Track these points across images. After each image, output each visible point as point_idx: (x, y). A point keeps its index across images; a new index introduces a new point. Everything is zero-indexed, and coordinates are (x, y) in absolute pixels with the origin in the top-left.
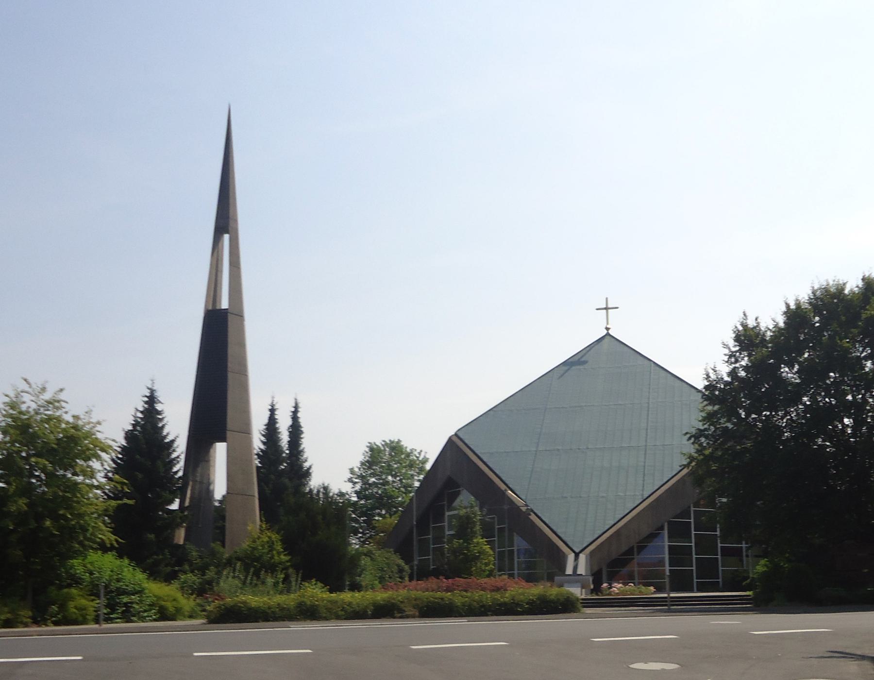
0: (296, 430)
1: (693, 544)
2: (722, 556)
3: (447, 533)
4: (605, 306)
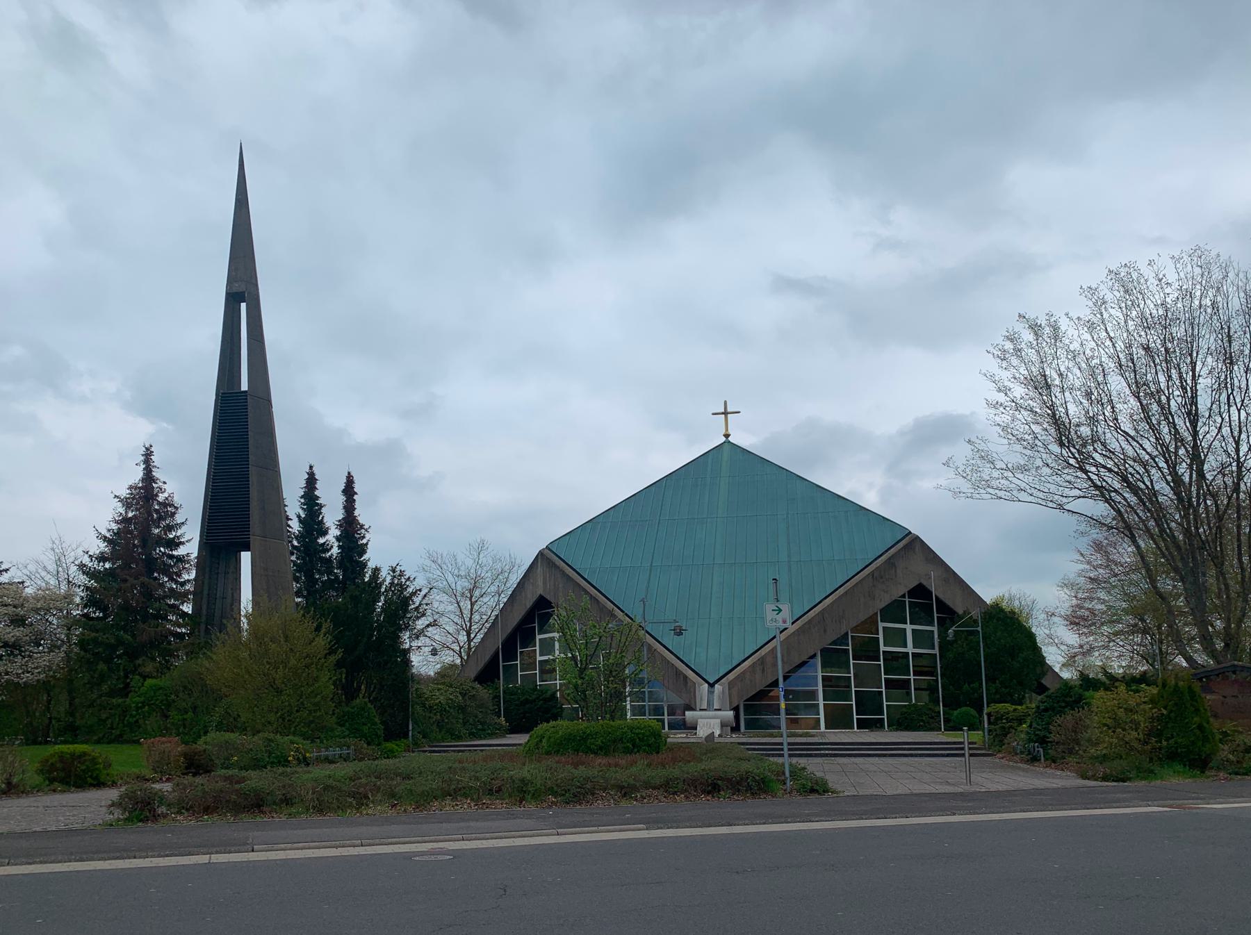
0: (350, 526)
1: (852, 675)
2: (886, 688)
3: (539, 658)
4: (723, 411)
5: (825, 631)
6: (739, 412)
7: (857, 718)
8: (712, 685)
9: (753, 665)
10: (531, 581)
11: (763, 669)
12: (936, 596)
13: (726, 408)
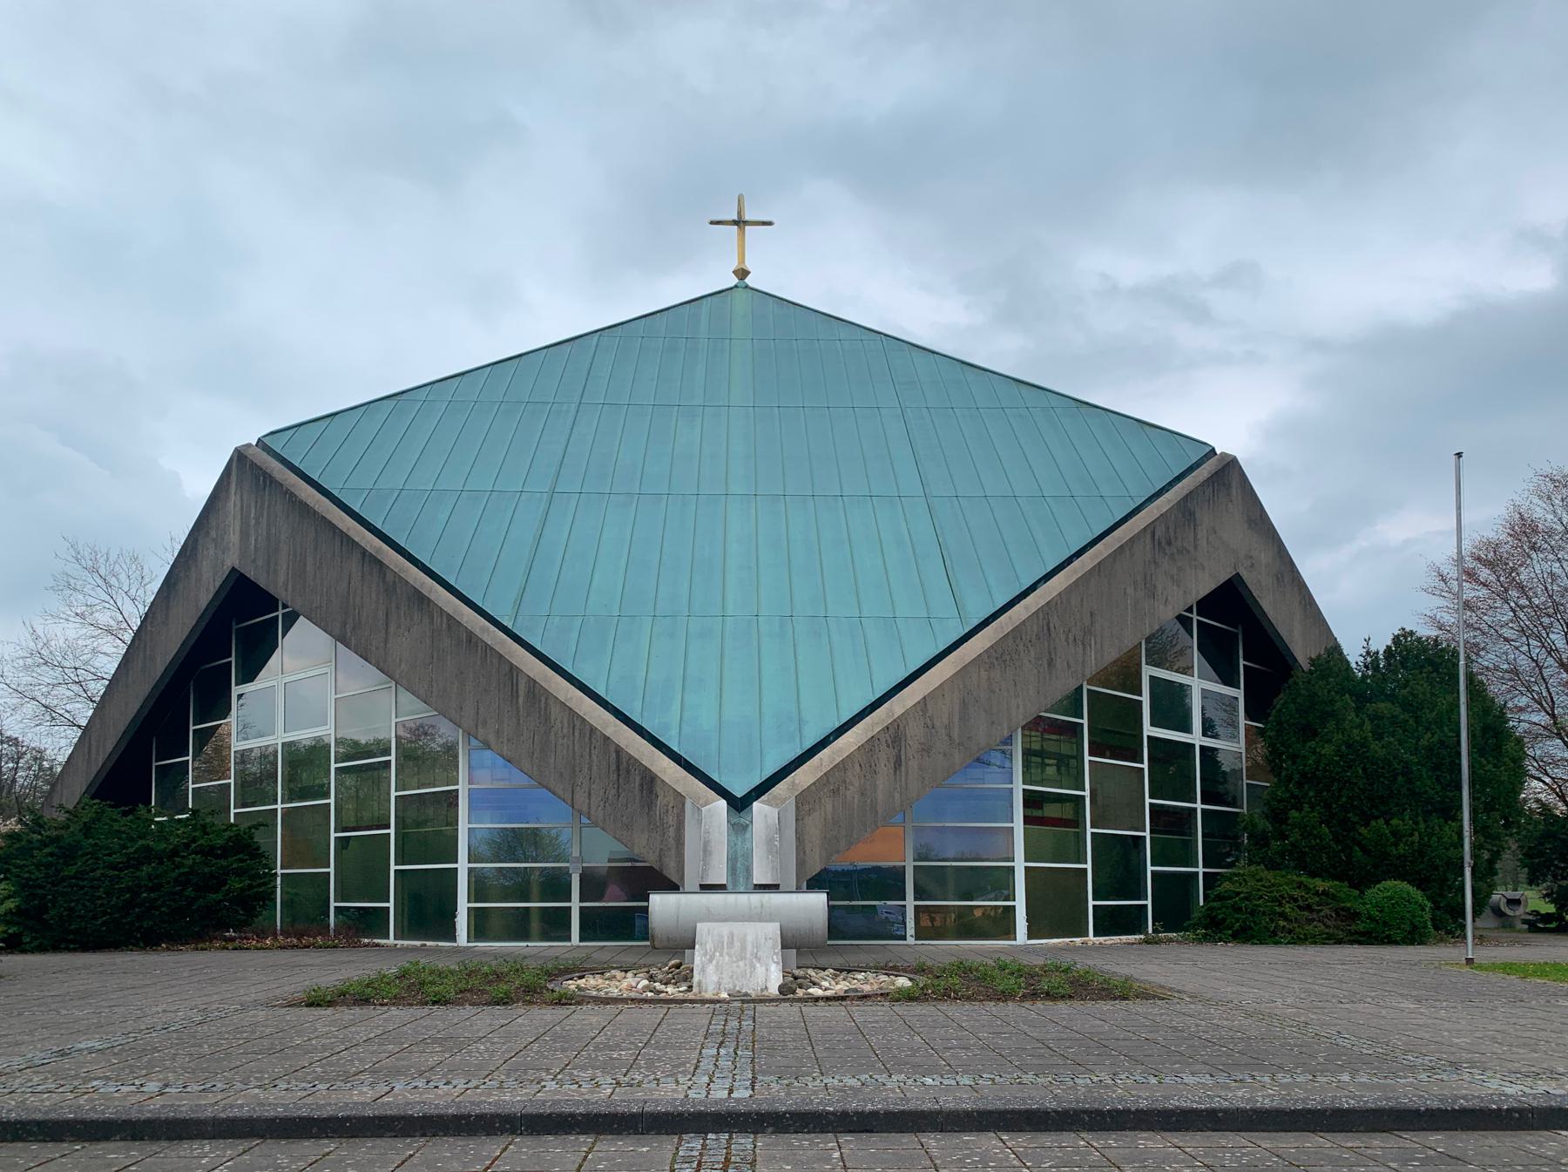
1: (1087, 793)
2: (1151, 832)
5: (1051, 663)
6: (769, 223)
7: (1094, 906)
8: (739, 805)
9: (870, 746)
10: (213, 534)
11: (899, 757)
12: (1192, 637)
13: (739, 213)
